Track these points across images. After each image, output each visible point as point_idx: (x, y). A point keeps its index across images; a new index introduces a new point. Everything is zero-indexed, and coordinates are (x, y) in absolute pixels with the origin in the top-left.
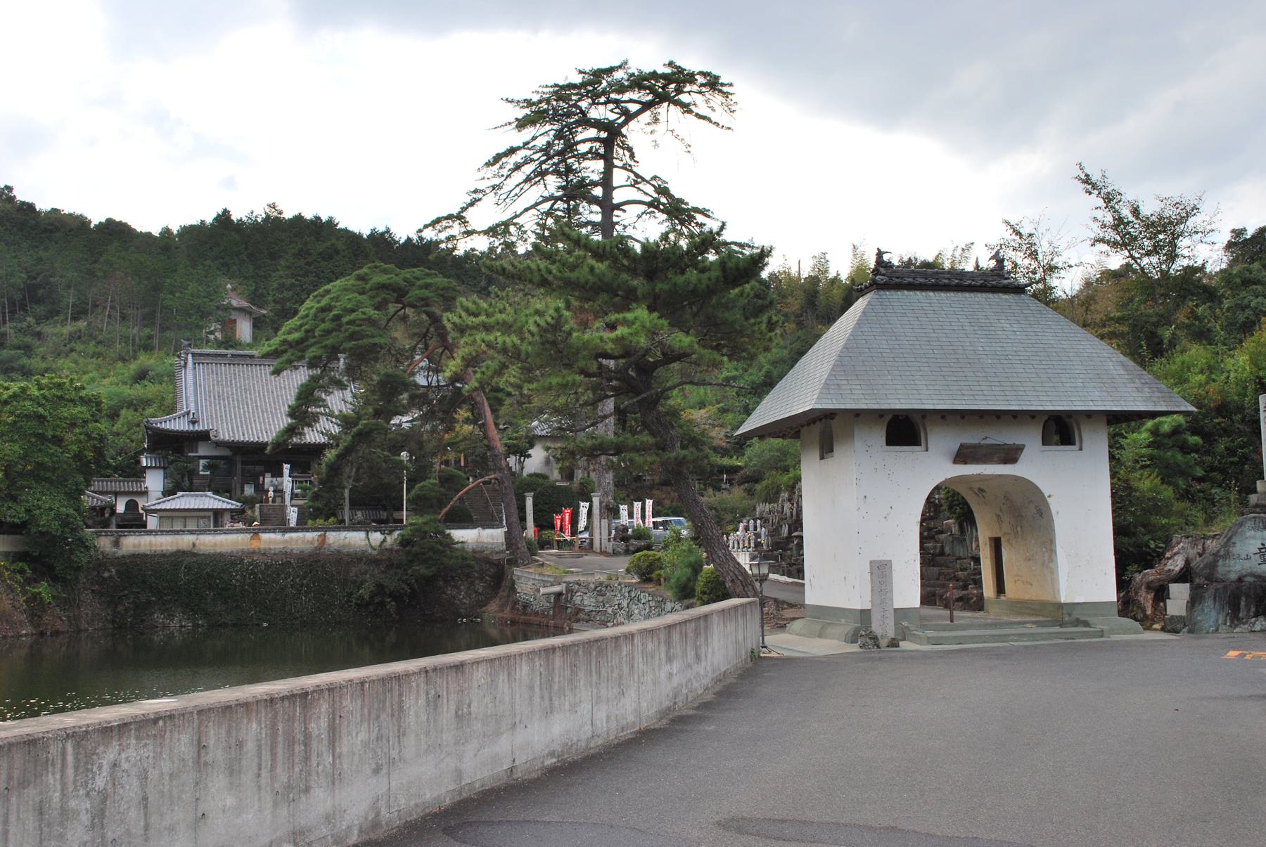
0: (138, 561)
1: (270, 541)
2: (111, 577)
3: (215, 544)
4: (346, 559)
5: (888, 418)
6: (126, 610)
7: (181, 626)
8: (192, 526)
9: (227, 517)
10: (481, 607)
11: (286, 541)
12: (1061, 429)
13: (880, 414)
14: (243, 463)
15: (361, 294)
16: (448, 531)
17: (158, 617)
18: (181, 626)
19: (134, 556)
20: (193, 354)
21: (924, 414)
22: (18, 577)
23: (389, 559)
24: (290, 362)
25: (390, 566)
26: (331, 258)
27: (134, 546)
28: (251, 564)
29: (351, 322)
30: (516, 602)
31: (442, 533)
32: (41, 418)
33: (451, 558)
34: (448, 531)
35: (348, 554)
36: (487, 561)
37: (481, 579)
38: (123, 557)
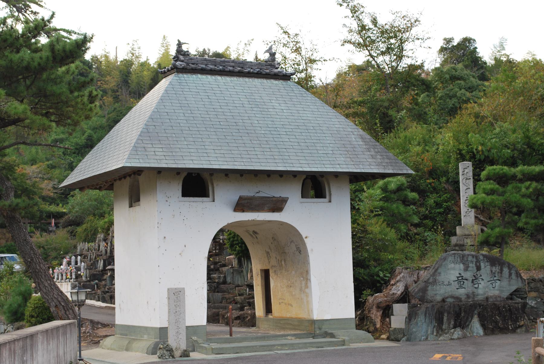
5: (184, 175)
12: (315, 185)
13: (177, 172)
21: (212, 172)
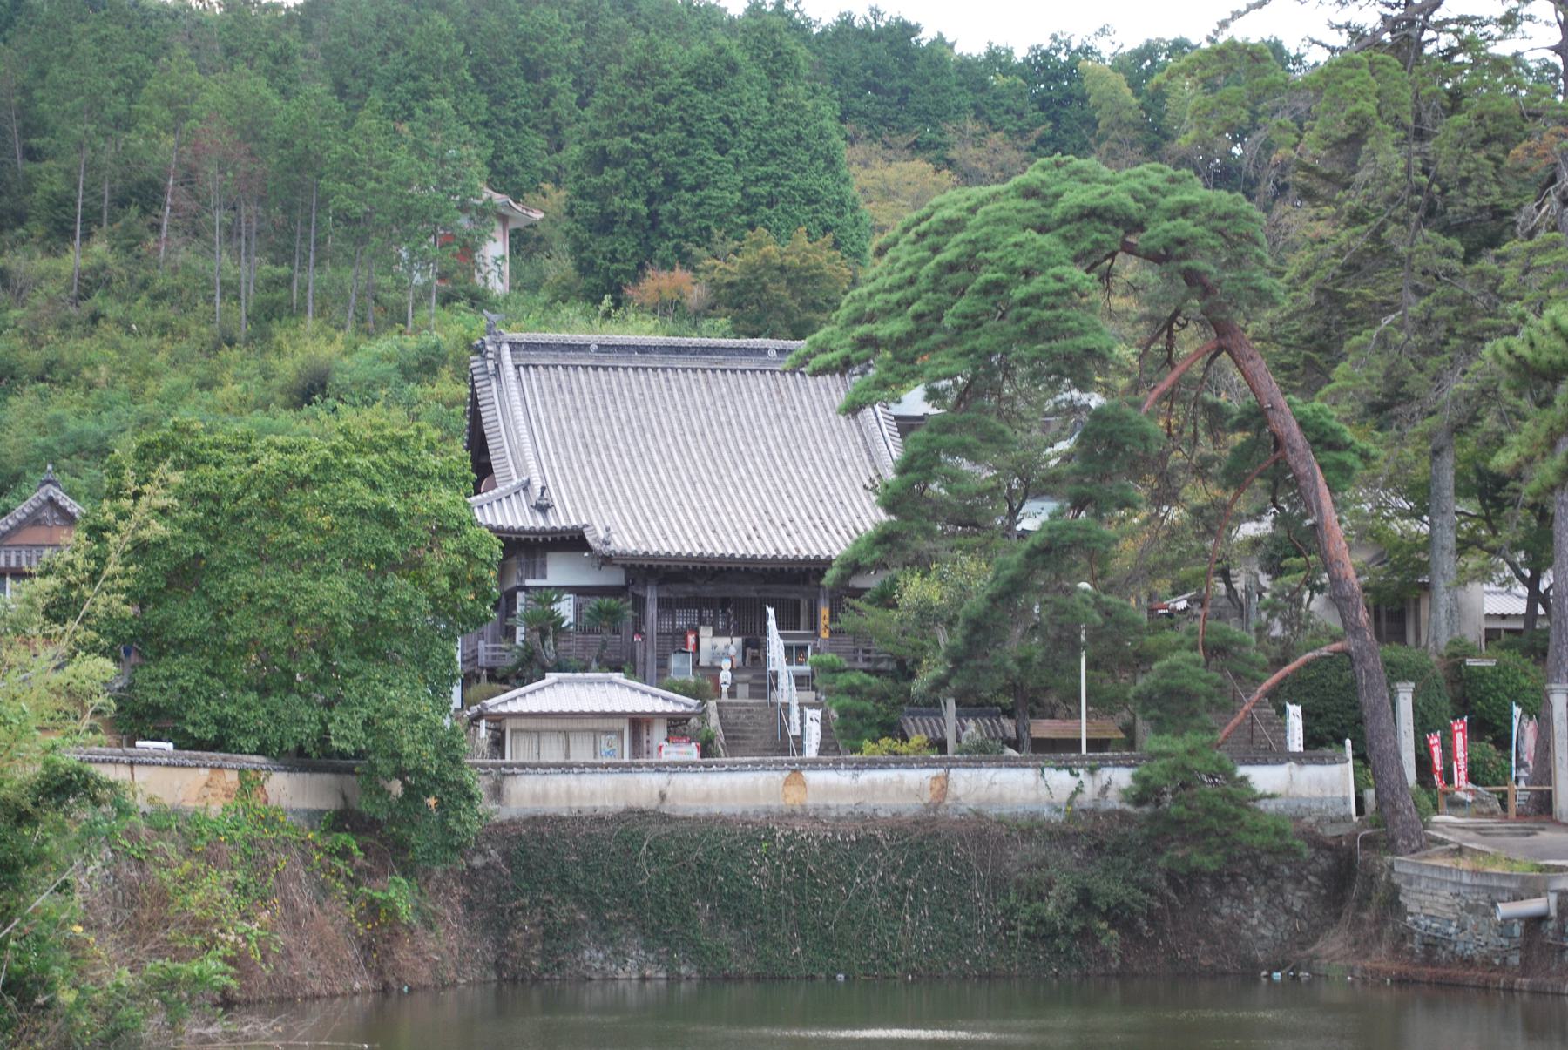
0: (546, 830)
1: (828, 790)
2: (487, 867)
3: (708, 796)
4: (989, 833)
6: (529, 941)
7: (644, 979)
8: (581, 752)
9: (659, 733)
10: (1303, 945)
11: (861, 790)
14: (665, 605)
15: (1042, 230)
16: (1242, 771)
17: (593, 956)
18: (644, 979)
19: (535, 820)
20: (513, 346)
22: (340, 864)
23: (1092, 834)
24: (883, 384)
25: (1099, 847)
26: (719, 83)
27: (534, 797)
28: (789, 840)
29: (1032, 300)
30: (1404, 936)
31: (1229, 775)
32: (387, 518)
33: (1254, 831)
34: (1242, 771)
35: (1000, 821)
36: (1318, 843)
37: (1298, 880)
38: (512, 822)
